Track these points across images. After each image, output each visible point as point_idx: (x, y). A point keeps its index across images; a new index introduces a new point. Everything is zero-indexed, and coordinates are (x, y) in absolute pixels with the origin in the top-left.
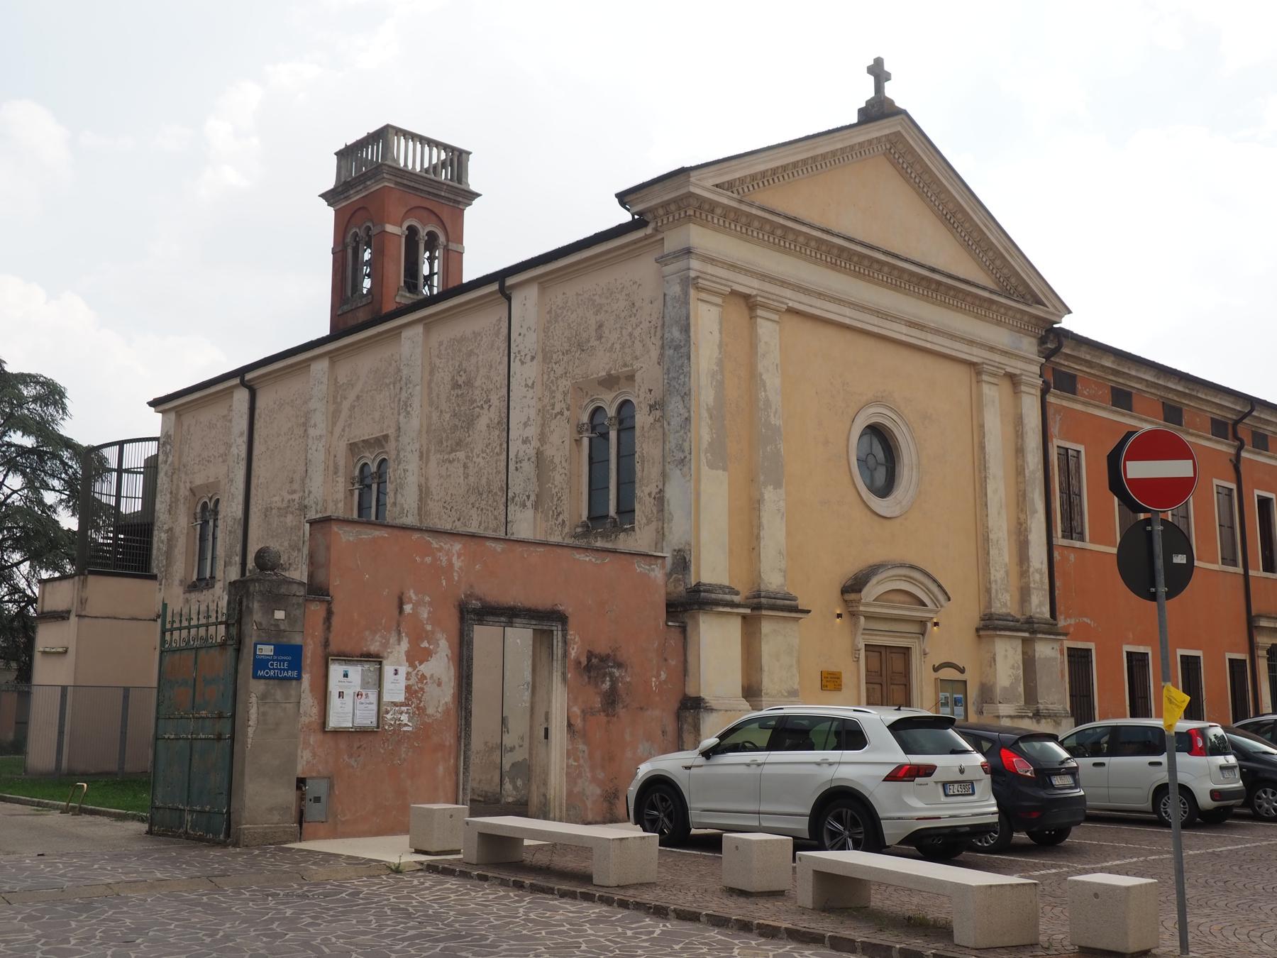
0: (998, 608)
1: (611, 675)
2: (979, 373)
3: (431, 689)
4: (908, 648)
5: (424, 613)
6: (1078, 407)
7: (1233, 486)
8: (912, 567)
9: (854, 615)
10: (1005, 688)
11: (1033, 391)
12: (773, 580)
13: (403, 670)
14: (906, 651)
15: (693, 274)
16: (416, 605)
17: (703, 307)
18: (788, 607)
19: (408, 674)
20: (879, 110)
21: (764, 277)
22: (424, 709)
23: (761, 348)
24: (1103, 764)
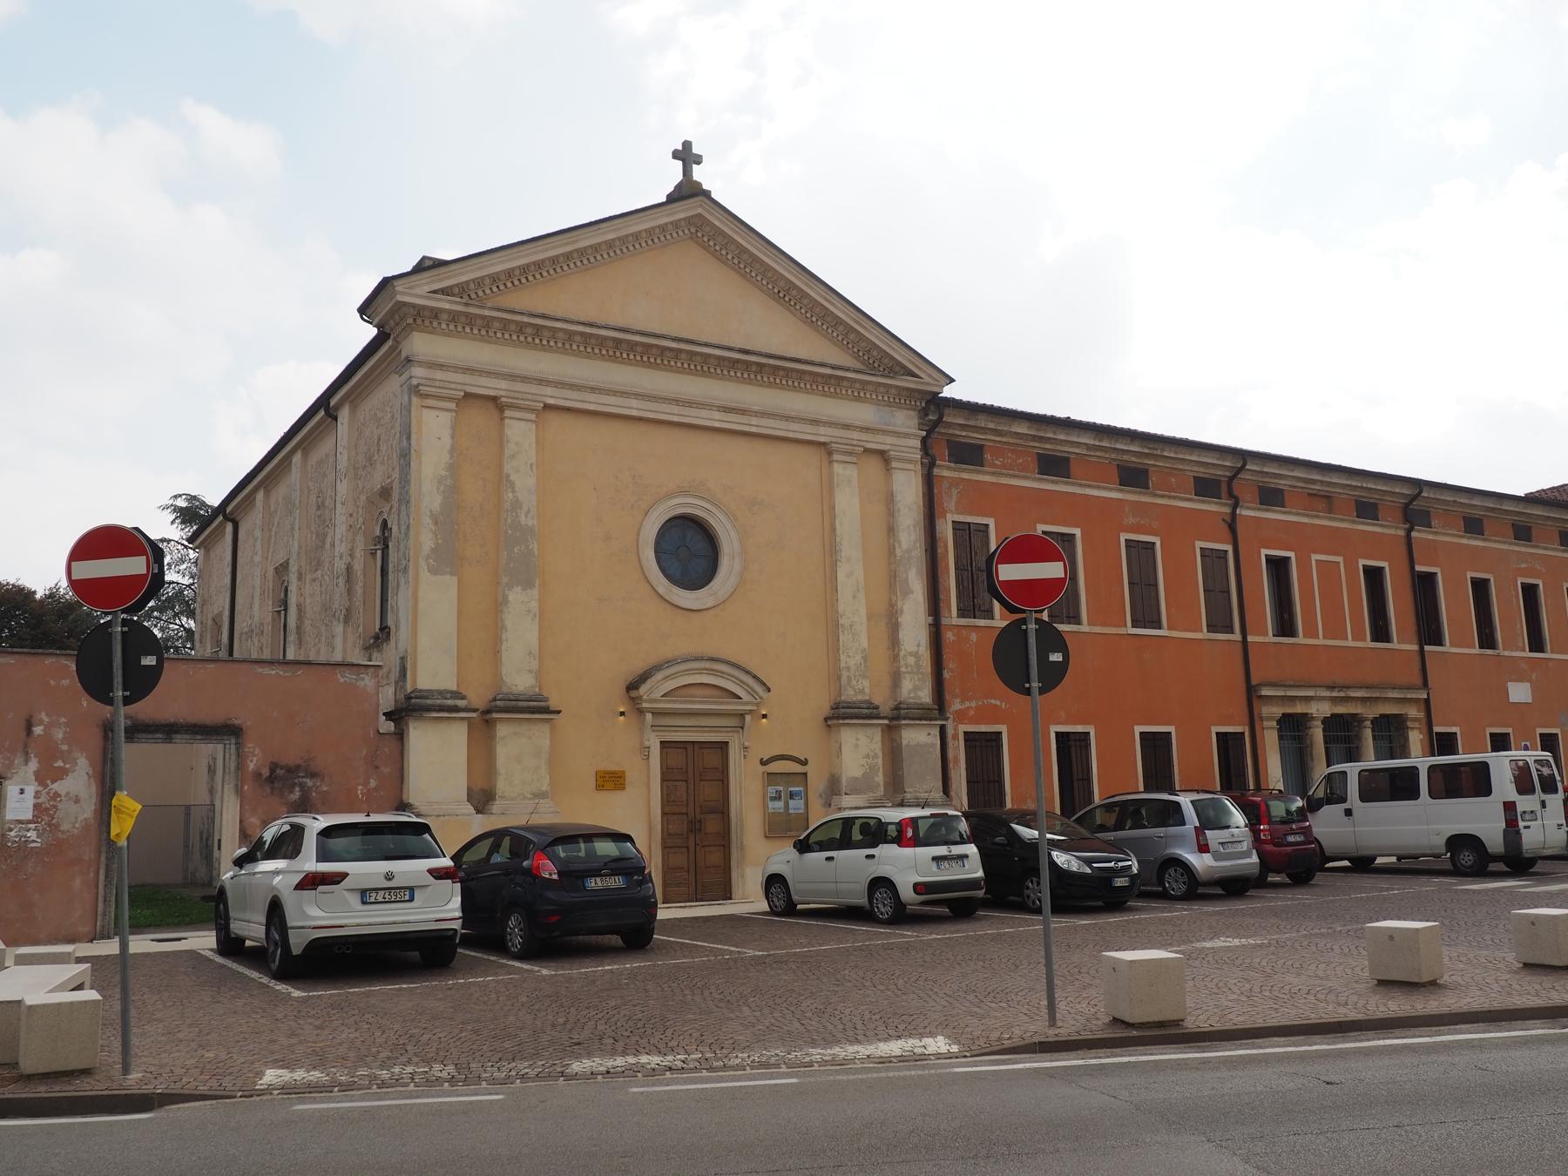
0: (850, 695)
1: (302, 786)
2: (830, 454)
3: (66, 807)
5: (59, 734)
6: (987, 478)
7: (1229, 548)
10: (855, 779)
11: (911, 466)
12: (519, 680)
13: (30, 790)
14: (723, 746)
15: (415, 382)
16: (48, 727)
17: (428, 416)
18: (534, 708)
19: (37, 792)
20: (689, 191)
21: (513, 377)
22: (57, 826)
23: (510, 449)
24: (872, 856)
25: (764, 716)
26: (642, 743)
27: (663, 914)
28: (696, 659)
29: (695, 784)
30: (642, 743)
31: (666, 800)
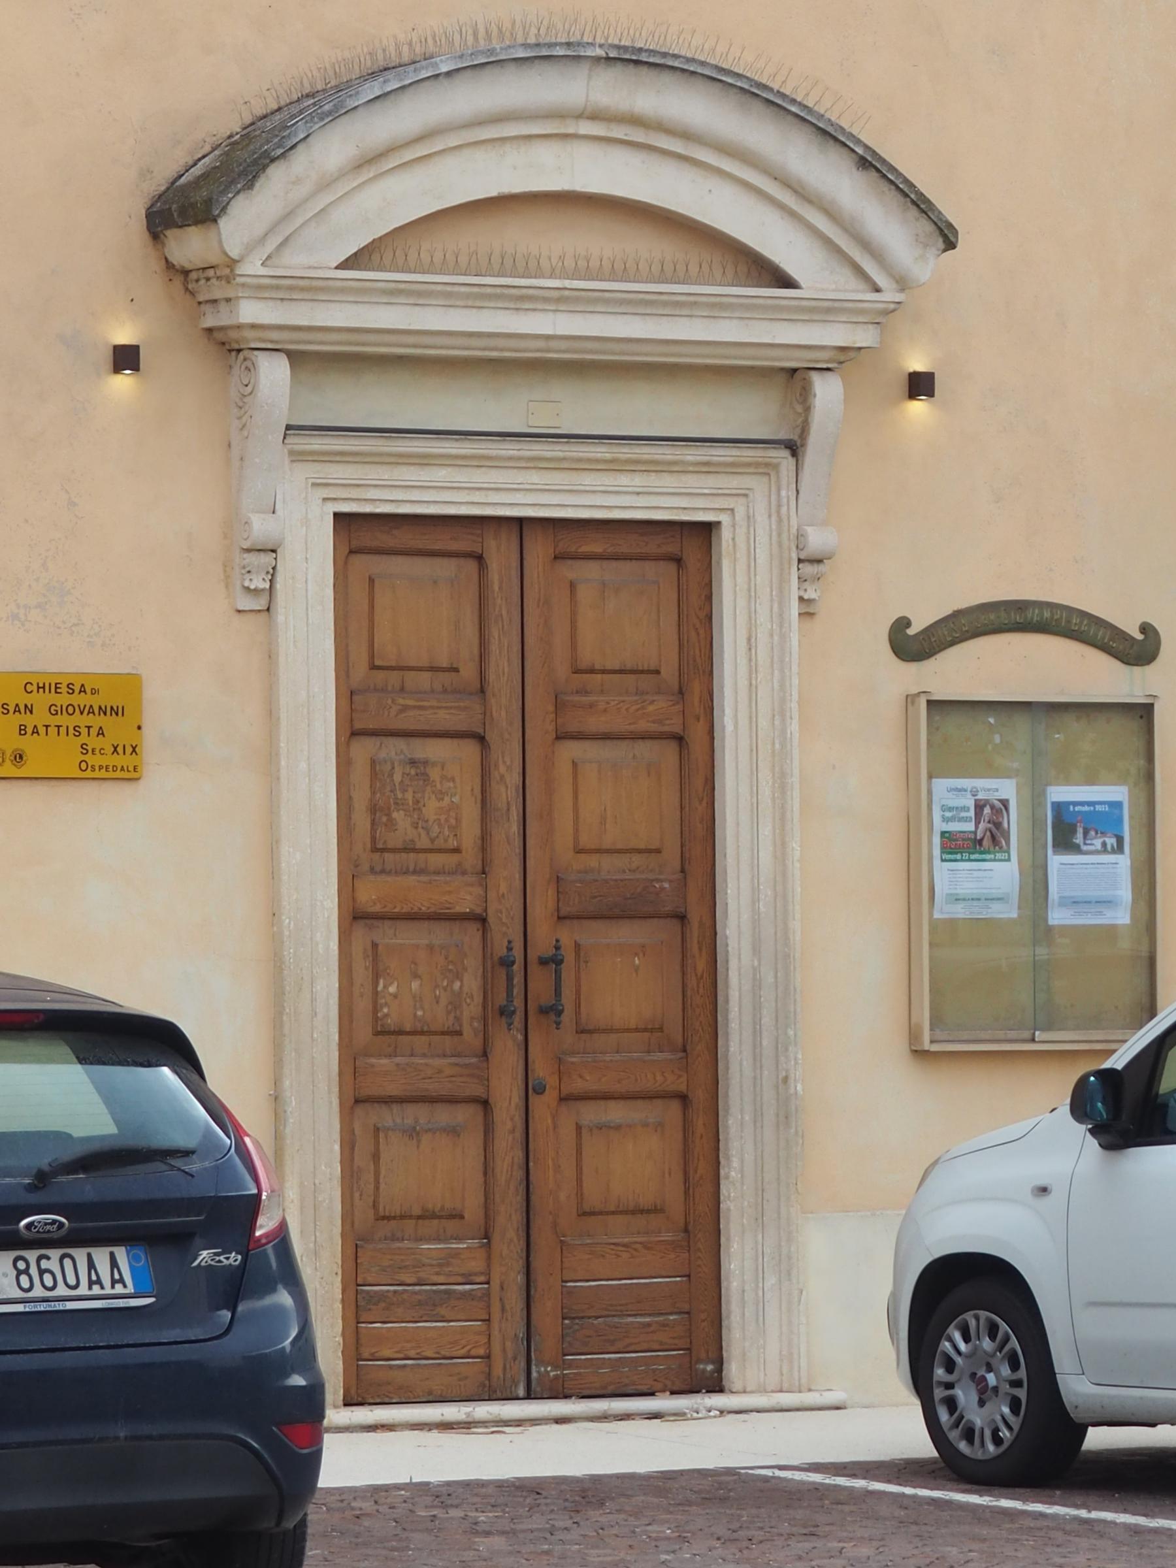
4: (706, 531)
8: (631, 60)
9: (229, 348)
14: (687, 547)
25: (920, 385)
26: (233, 522)
27: (358, 1456)
28: (541, 56)
29: (531, 728)
30: (233, 522)
31: (369, 845)
